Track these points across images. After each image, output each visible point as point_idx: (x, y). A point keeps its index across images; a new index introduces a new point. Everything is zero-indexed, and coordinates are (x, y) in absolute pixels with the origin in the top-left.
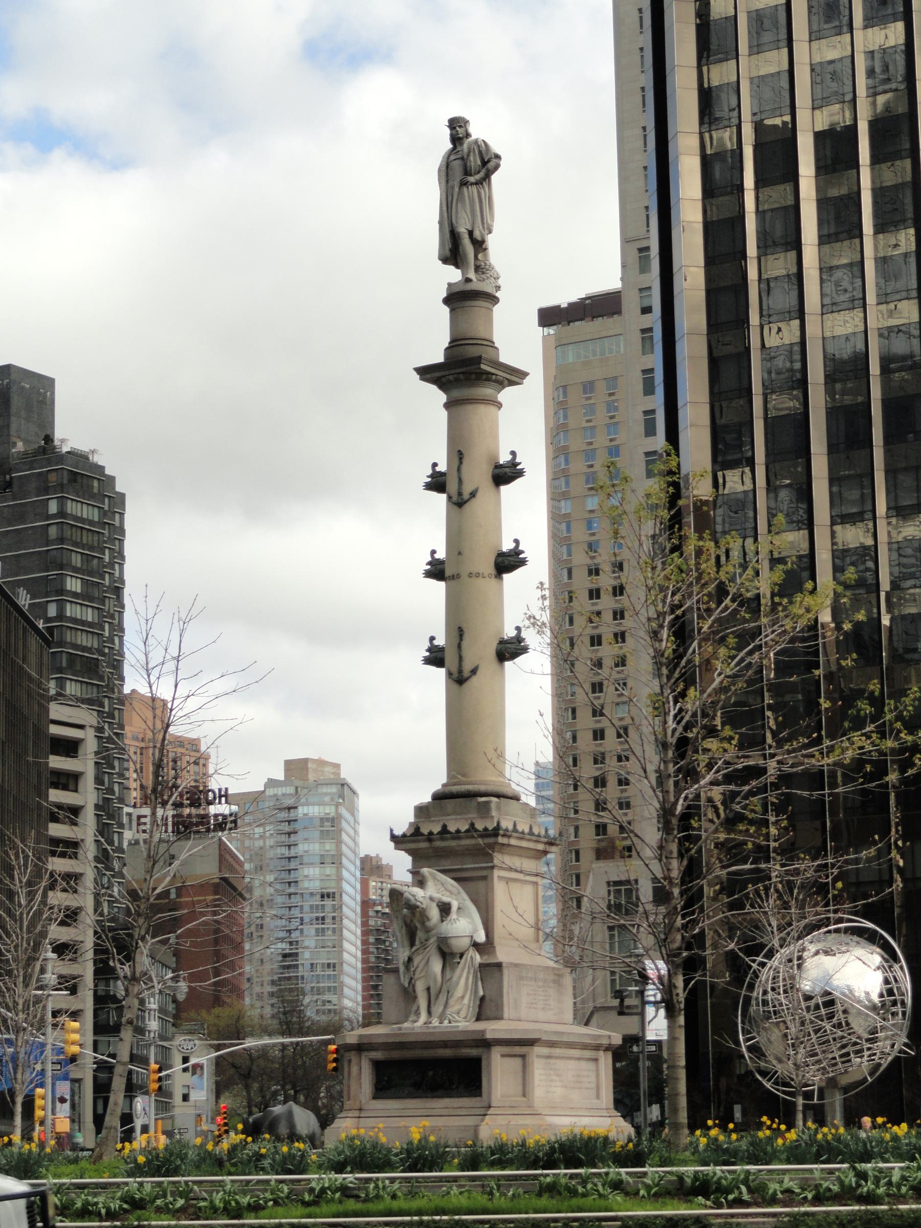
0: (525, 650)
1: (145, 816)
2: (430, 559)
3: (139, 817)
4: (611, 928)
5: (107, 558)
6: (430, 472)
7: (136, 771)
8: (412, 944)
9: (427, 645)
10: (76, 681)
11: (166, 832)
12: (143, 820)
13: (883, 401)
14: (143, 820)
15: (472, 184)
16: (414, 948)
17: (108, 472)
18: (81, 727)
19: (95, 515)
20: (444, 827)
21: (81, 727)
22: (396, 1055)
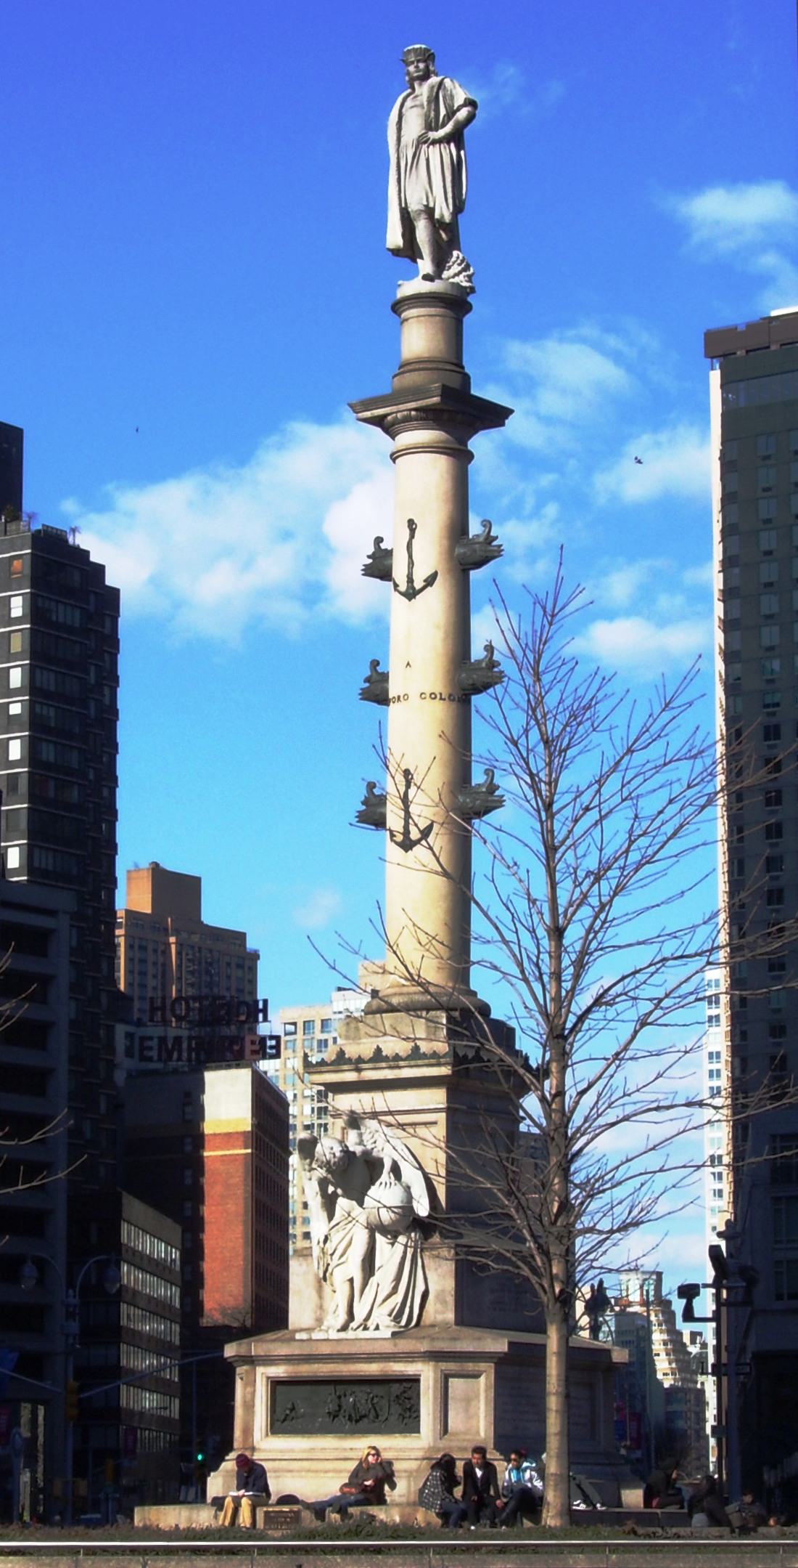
0: (499, 803)
1: (151, 1038)
2: (368, 673)
3: (143, 1039)
4: (777, 1200)
5: (92, 678)
6: (371, 550)
7: (155, 976)
8: (331, 1216)
9: (363, 793)
10: (47, 849)
11: (179, 1059)
12: (149, 1043)
13: (723, 415)
14: (149, 1043)
15: (434, 142)
16: (333, 1222)
17: (94, 558)
18: (51, 913)
19: (75, 618)
20: (379, 1050)
21: (51, 913)
22: (306, 1370)
